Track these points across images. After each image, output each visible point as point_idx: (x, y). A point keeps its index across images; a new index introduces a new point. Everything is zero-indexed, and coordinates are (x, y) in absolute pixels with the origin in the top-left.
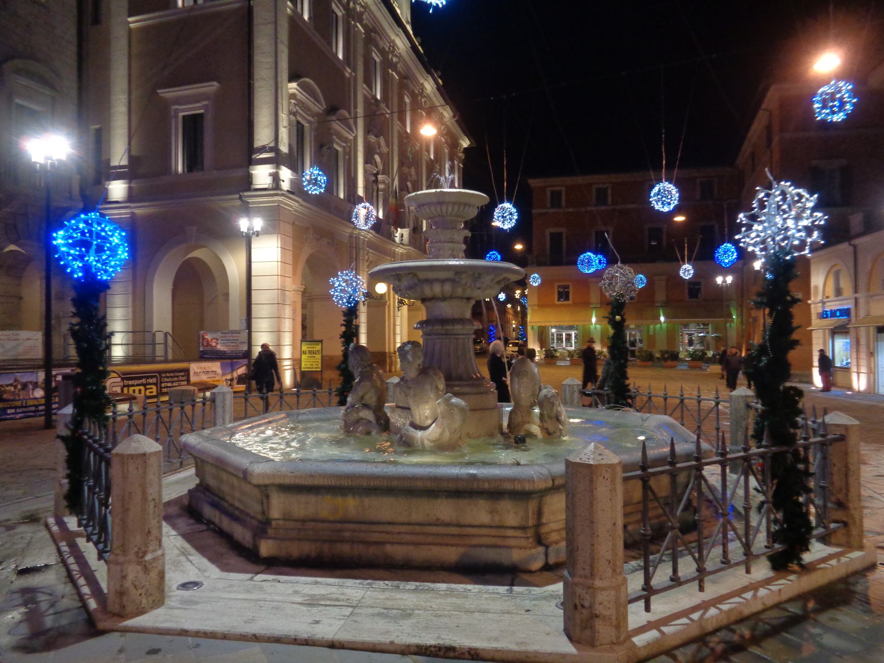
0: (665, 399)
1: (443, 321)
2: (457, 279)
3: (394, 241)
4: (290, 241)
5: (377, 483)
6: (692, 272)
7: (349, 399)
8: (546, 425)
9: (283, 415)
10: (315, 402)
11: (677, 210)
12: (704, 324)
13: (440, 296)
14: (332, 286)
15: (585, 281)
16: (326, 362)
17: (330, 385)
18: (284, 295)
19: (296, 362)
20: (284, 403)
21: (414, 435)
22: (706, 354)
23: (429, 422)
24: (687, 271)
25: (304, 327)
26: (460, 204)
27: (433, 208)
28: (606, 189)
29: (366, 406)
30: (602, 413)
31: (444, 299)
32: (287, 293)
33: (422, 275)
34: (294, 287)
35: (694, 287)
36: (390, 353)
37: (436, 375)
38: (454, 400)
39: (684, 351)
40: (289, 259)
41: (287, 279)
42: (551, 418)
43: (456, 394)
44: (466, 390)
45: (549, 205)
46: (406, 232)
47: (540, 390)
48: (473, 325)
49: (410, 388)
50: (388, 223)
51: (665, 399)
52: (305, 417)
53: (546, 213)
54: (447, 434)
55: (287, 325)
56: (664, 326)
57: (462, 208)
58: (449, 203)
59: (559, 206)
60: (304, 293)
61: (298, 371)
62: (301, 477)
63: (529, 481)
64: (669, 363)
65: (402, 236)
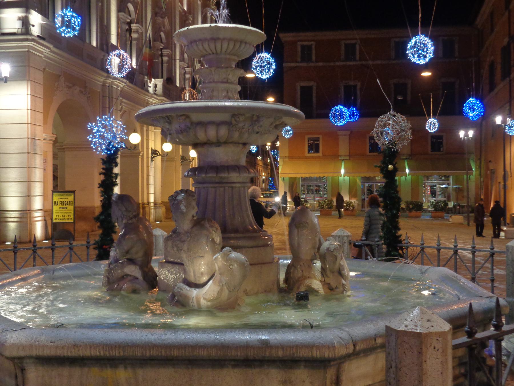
0: (439, 250)
1: (217, 168)
2: (234, 122)
3: (148, 91)
4: (40, 90)
5: (154, 353)
6: (437, 125)
7: (112, 254)
8: (327, 280)
9: (37, 271)
10: (71, 255)
11: (426, 67)
12: (445, 176)
13: (215, 140)
14: (90, 132)
15: (334, 134)
16: (80, 214)
17: (88, 237)
18: (34, 145)
19: (47, 213)
20: (37, 257)
21: (189, 294)
22: (447, 205)
23: (205, 279)
24: (432, 125)
25: (55, 178)
26: (236, 41)
27: (206, 45)
28: (356, 44)
29: (131, 261)
30: (374, 266)
31: (218, 143)
32: (38, 142)
33: (195, 117)
34: (45, 136)
35: (437, 141)
36: (143, 204)
37: (212, 227)
38: (233, 255)
39: (428, 201)
40: (40, 106)
41: (38, 128)
42: (332, 272)
43: (235, 248)
44: (241, 243)
45: (299, 59)
46: (160, 82)
47: (320, 244)
48: (249, 172)
49: (183, 241)
50: (141, 73)
51: (439, 250)
52: (61, 273)
53: (297, 67)
54: (226, 292)
55: (38, 175)
56: (409, 177)
57: (238, 45)
58: (224, 39)
59: (309, 60)
60: (55, 142)
61: (49, 223)
62: (63, 347)
63: (329, 348)
64: (414, 213)
65: (156, 86)
